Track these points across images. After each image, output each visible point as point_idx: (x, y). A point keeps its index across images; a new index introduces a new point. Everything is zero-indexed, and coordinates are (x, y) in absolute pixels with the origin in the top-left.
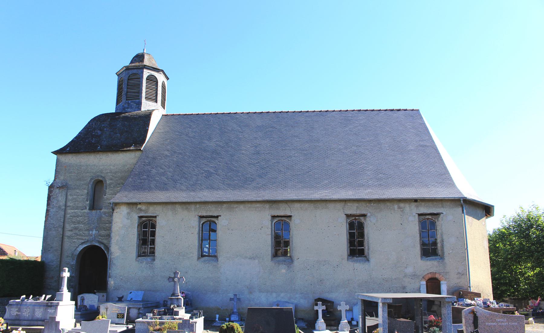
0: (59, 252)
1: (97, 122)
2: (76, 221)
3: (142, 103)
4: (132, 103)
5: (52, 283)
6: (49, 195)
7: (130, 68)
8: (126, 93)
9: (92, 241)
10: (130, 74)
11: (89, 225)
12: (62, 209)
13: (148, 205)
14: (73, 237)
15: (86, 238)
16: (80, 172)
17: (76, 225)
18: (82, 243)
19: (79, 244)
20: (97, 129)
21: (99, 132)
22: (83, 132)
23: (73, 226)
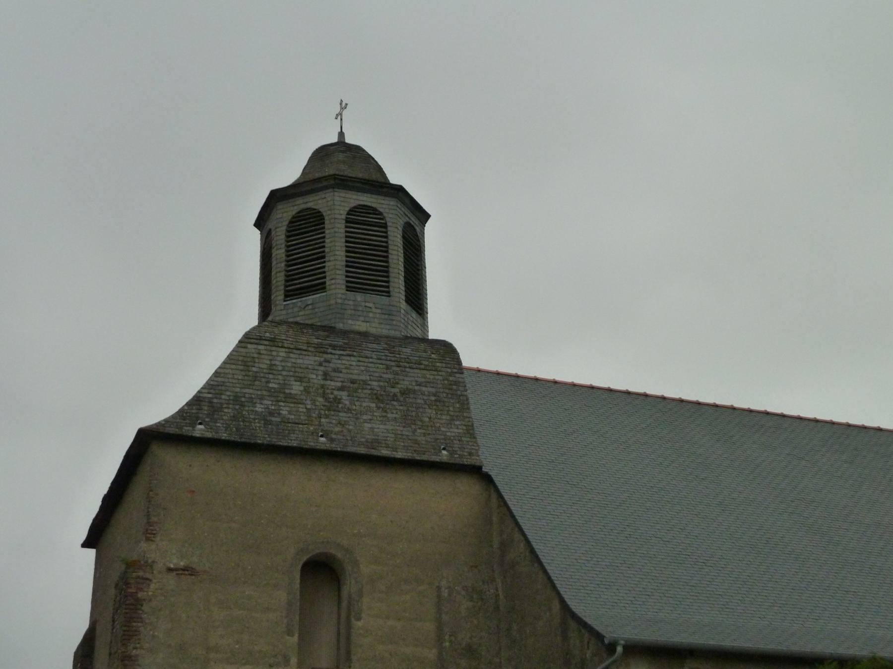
22: (230, 371)
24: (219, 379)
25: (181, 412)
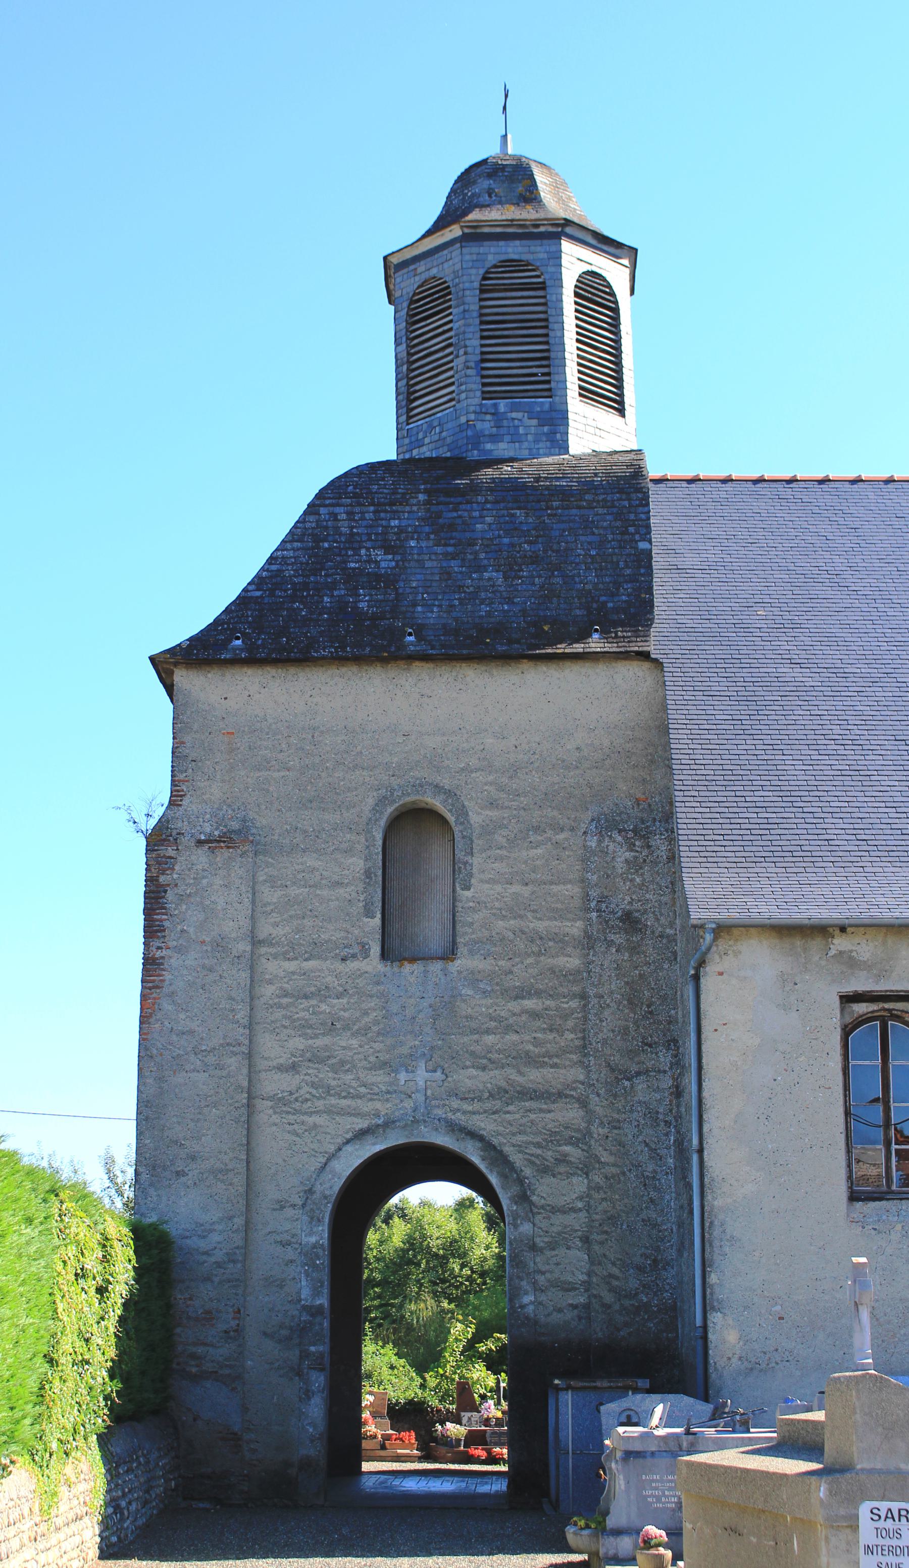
0: (239, 1181)
1: (360, 504)
2: (314, 1020)
3: (570, 416)
4: (514, 415)
5: (205, 1344)
6: (150, 881)
7: (486, 230)
8: (478, 358)
9: (416, 1121)
10: (488, 265)
11: (389, 1041)
12: (235, 953)
13: (890, 941)
14: (307, 1100)
15: (378, 1105)
16: (317, 760)
17: (316, 1036)
18: (361, 1135)
19: (340, 1140)
20: (369, 544)
21: (386, 561)
22: (291, 553)
23: (298, 1043)
24: (274, 567)
25: (217, 621)
